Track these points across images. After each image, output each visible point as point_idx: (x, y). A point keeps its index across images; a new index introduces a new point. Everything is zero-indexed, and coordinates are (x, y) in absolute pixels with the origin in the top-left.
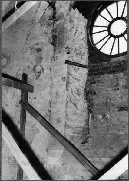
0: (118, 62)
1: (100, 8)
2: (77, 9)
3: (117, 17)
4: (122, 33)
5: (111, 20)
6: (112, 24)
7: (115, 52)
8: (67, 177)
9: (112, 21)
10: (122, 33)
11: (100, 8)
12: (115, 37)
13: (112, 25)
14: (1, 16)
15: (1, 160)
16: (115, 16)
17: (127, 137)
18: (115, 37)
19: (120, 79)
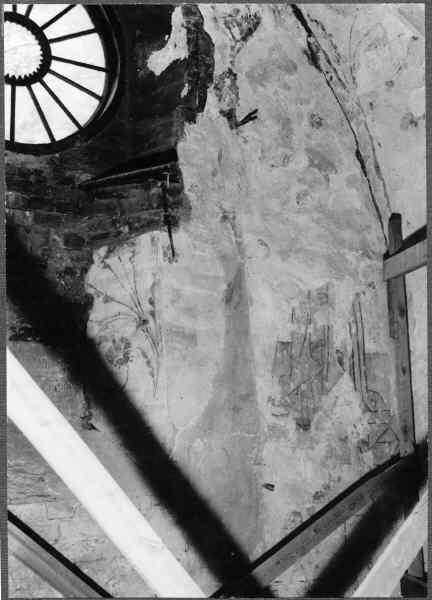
0: (19, 169)
1: (115, 41)
2: (305, 2)
3: (54, 54)
4: (41, 58)
5: (49, 33)
6: (33, 33)
7: (97, 82)
8: (388, 14)
9: (43, 76)
10: (41, 58)
11: (115, 41)
12: (45, 68)
13: (29, 32)
14: (300, 3)
15: (383, 2)
16: (56, 49)
17: (12, 493)
18: (45, 68)
19: (71, 515)
